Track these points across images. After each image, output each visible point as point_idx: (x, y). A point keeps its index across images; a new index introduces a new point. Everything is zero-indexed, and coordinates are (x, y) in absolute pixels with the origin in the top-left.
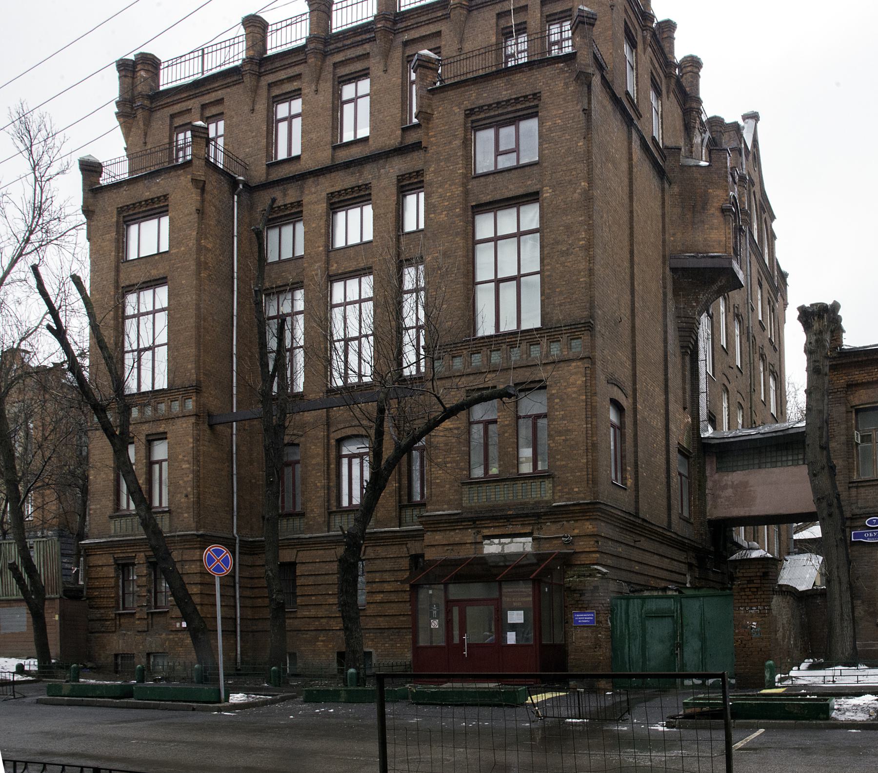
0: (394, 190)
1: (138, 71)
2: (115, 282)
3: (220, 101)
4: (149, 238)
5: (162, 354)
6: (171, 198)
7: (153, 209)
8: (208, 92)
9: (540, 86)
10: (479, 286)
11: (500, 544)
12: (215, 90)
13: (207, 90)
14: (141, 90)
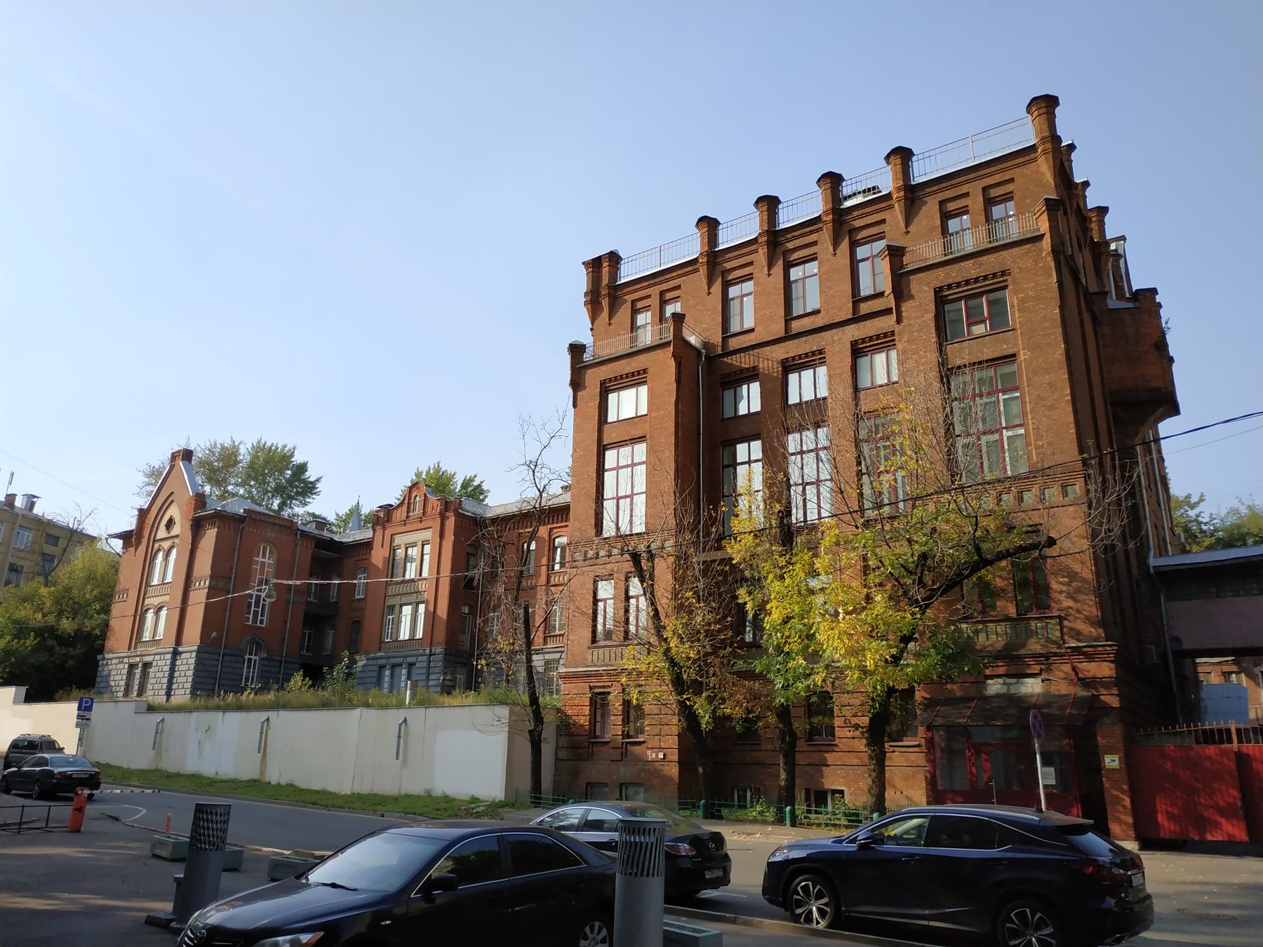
0: (849, 353)
1: (603, 269)
2: (600, 439)
3: (678, 287)
4: (628, 404)
5: (640, 501)
6: (650, 371)
7: (634, 379)
8: (667, 280)
9: (1009, 265)
10: (589, 372)
11: (1005, 684)
12: (673, 278)
13: (664, 281)
14: (606, 286)
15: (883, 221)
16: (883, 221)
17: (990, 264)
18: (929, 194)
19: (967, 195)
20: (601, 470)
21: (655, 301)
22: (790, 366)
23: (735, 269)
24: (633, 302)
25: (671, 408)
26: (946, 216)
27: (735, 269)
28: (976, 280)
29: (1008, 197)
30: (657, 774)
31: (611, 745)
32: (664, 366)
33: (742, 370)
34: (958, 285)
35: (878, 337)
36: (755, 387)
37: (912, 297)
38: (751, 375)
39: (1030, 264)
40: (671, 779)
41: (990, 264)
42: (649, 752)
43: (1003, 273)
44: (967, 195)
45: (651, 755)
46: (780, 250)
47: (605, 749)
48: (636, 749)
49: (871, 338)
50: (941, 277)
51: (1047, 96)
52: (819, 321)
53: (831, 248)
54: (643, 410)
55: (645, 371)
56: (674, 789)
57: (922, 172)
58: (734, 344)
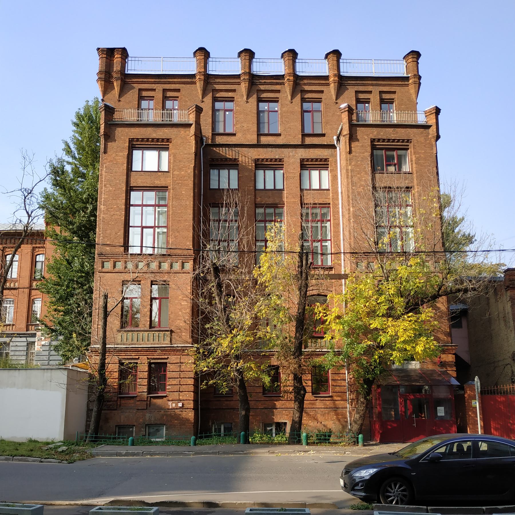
3: (178, 90)
7: (160, 145)
9: (411, 137)
12: (175, 83)
13: (168, 84)
15: (322, 92)
16: (322, 92)
17: (401, 134)
18: (350, 85)
19: (370, 92)
20: (128, 205)
21: (159, 95)
22: (260, 165)
23: (221, 91)
24: (140, 90)
25: (190, 171)
26: (141, 98)
27: (221, 91)
28: (394, 141)
29: (175, 98)
30: (177, 417)
31: (138, 399)
32: (186, 143)
33: (226, 159)
34: (384, 140)
35: (317, 160)
36: (234, 173)
37: (358, 140)
38: (232, 164)
39: (422, 139)
40: (188, 420)
41: (401, 134)
42: (170, 403)
43: (408, 141)
44: (370, 92)
45: (172, 405)
46: (255, 88)
47: (132, 401)
48: (158, 401)
49: (312, 160)
50: (375, 133)
51: (412, 52)
52: (279, 141)
53: (289, 97)
54: (165, 167)
55: (168, 140)
56: (191, 426)
57: (347, 70)
58: (219, 140)
